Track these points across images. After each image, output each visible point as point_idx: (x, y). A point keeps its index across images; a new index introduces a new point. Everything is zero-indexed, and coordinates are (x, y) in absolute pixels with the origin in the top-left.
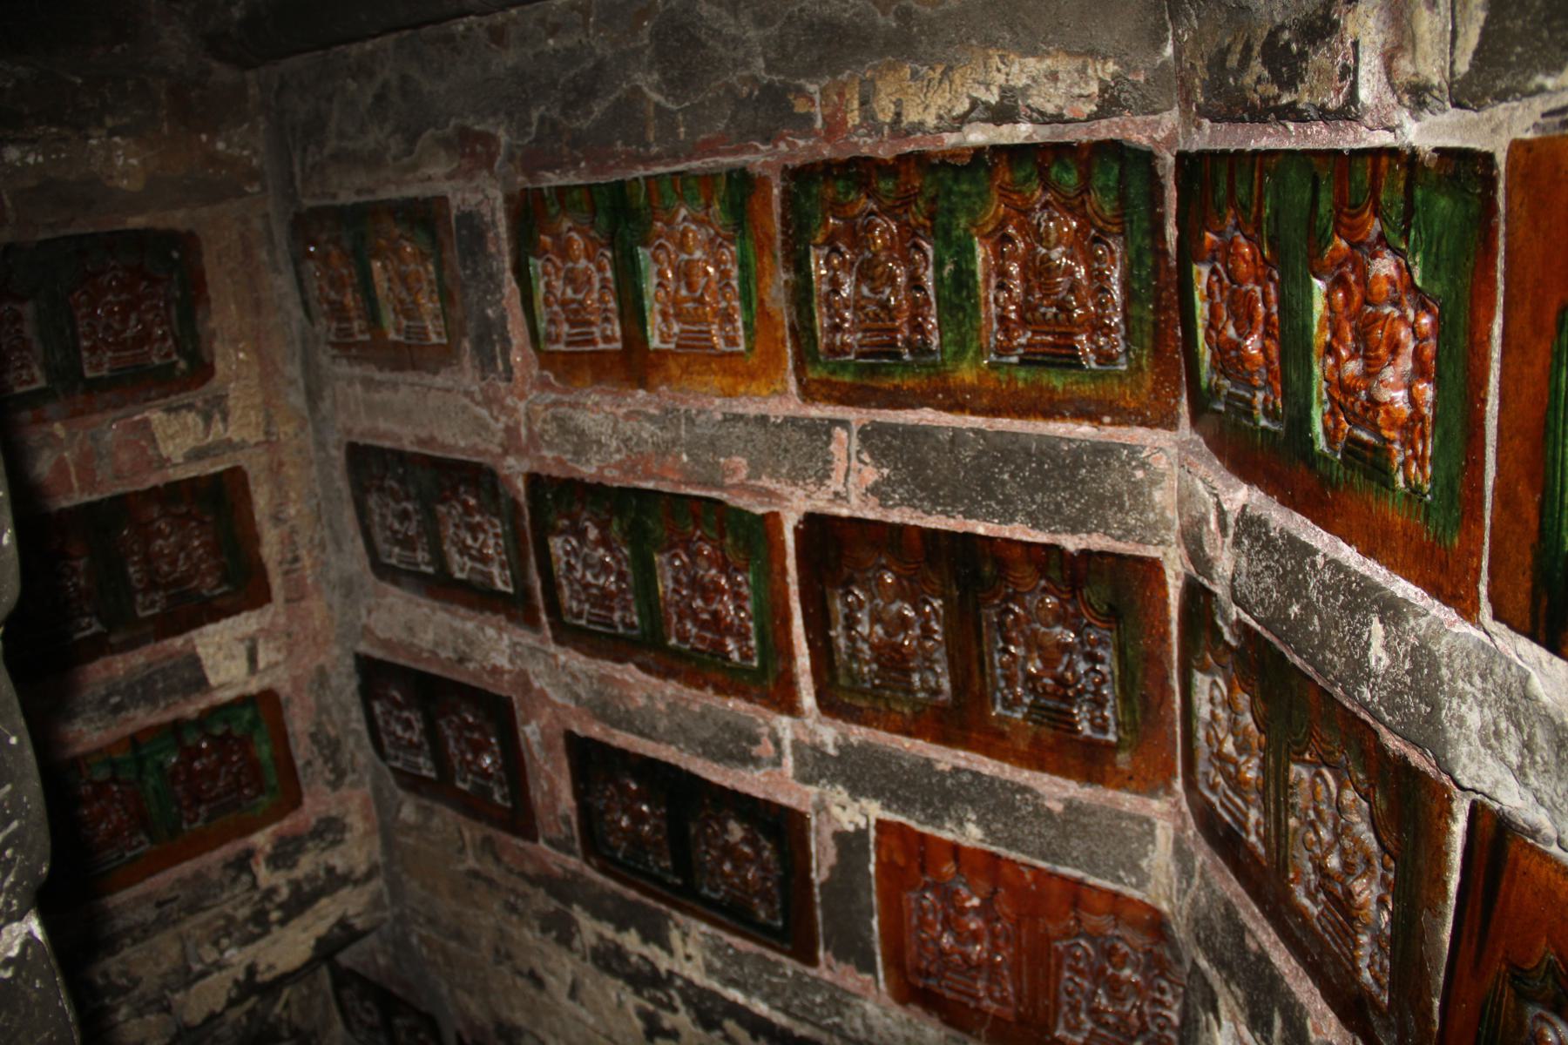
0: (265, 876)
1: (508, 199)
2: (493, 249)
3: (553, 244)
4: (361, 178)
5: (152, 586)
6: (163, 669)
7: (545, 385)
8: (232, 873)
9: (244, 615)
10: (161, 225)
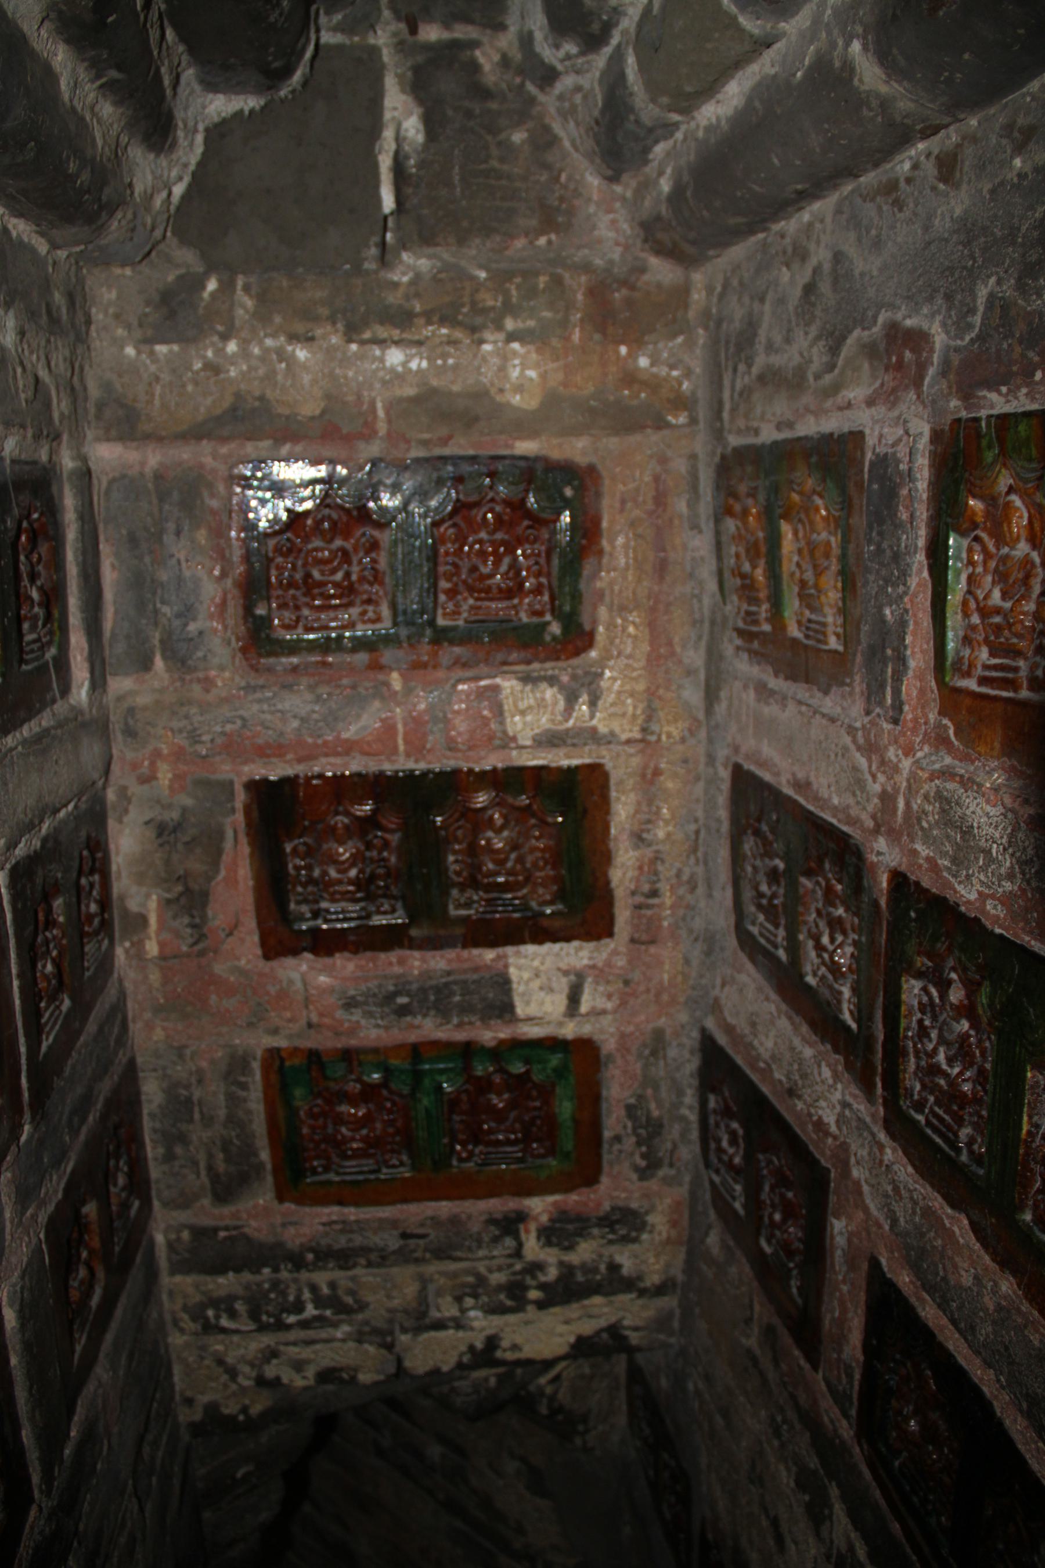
0: (532, 1247)
1: (936, 436)
2: (904, 516)
3: (987, 514)
4: (781, 407)
5: (473, 882)
6: (465, 982)
7: (941, 741)
8: (495, 1231)
9: (576, 943)
10: (555, 455)
